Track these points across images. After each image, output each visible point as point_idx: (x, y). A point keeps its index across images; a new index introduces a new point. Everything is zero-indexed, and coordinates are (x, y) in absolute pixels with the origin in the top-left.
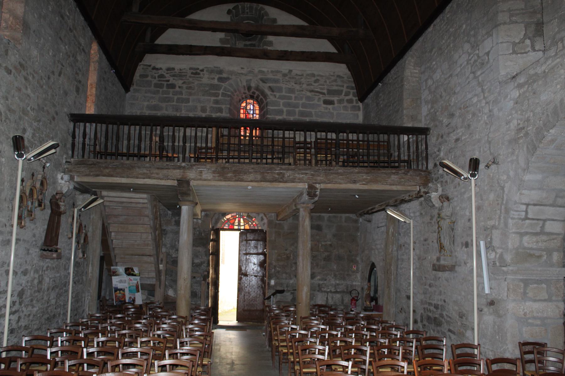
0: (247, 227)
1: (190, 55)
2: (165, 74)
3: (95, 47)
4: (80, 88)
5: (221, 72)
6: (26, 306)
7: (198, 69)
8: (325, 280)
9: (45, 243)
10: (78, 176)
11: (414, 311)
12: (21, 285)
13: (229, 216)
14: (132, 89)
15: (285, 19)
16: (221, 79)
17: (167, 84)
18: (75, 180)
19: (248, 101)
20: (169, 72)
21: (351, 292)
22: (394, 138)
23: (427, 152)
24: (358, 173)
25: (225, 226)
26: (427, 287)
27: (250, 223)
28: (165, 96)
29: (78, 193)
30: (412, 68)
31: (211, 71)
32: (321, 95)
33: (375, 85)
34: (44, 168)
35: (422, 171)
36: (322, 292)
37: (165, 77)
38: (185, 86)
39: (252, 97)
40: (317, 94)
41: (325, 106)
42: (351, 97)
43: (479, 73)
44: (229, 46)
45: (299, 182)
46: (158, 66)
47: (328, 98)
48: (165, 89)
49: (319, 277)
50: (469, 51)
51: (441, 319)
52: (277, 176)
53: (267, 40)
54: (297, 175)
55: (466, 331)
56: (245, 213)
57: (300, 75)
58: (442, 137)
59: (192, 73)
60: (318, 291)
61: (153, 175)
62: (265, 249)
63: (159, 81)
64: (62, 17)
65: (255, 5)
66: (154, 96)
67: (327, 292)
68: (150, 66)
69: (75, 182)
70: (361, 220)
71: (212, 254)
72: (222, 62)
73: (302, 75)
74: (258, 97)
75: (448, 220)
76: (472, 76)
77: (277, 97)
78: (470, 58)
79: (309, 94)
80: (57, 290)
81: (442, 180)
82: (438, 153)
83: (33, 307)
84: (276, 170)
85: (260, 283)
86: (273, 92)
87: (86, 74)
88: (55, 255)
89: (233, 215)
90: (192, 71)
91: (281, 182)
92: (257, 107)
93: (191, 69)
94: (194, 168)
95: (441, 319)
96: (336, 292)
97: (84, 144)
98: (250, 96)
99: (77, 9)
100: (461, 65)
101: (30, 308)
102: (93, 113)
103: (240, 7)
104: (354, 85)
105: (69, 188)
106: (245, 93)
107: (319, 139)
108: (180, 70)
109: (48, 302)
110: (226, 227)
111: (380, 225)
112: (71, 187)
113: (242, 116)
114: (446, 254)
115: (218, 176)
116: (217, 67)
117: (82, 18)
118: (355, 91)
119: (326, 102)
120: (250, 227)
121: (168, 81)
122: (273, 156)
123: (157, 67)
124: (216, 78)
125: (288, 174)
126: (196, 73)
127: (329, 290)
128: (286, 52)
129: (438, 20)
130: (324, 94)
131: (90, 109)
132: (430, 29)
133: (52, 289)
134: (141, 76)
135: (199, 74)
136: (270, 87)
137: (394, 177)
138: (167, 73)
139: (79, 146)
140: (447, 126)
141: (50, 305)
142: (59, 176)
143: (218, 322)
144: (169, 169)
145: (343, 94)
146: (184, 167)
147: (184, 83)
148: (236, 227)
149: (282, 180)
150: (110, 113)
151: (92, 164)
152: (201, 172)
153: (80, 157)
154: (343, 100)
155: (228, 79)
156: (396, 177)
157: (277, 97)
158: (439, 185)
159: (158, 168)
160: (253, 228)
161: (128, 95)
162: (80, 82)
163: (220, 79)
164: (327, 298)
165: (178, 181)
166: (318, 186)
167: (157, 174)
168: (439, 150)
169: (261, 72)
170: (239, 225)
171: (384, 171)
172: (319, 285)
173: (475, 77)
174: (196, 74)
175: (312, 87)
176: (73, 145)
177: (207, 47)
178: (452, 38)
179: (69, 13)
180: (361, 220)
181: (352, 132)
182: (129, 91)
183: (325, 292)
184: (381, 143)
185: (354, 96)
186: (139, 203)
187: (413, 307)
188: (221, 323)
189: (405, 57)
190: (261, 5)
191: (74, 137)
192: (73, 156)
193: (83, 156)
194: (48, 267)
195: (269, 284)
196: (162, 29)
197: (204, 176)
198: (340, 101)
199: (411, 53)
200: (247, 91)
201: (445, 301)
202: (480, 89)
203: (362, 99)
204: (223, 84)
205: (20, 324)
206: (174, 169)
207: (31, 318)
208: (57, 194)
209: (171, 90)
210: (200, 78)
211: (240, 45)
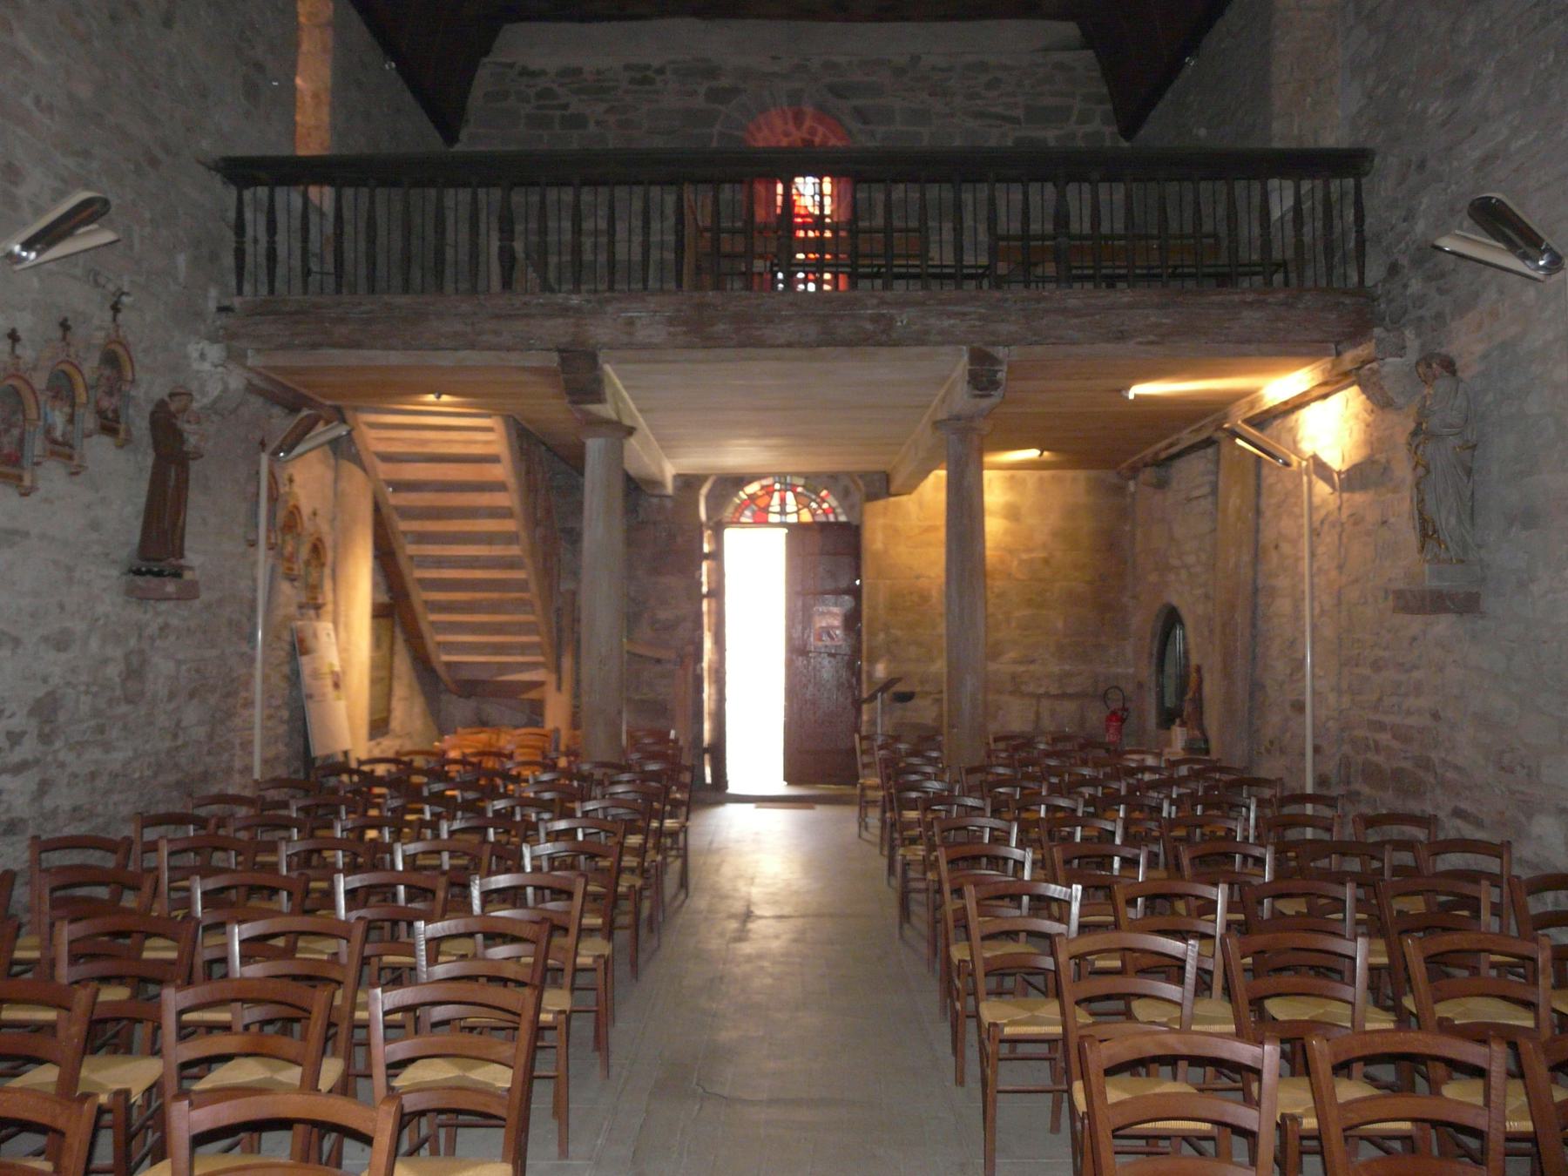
0: (806, 517)
2: (555, 86)
5: (712, 72)
6: (79, 747)
7: (648, 67)
8: (1033, 662)
9: (144, 550)
10: (258, 351)
11: (1317, 750)
12: (45, 680)
13: (753, 488)
16: (715, 95)
17: (563, 116)
18: (250, 362)
21: (1106, 694)
24: (1130, 306)
25: (741, 514)
26: (1367, 671)
27: (814, 505)
29: (277, 411)
33: (1175, 68)
34: (116, 308)
35: (1345, 293)
36: (1023, 695)
45: (942, 344)
46: (535, 64)
49: (1012, 655)
51: (1421, 773)
52: (869, 326)
54: (932, 321)
55: (1530, 817)
56: (798, 474)
57: (942, 70)
60: (1012, 693)
61: (485, 338)
62: (859, 577)
63: (539, 107)
67: (1039, 697)
68: (511, 66)
69: (250, 369)
70: (1132, 486)
71: (709, 595)
75: (1453, 441)
80: (213, 700)
81: (1421, 312)
83: (107, 747)
85: (844, 674)
86: (866, 122)
87: (287, 52)
88: (171, 587)
89: (765, 482)
91: (881, 345)
93: (627, 67)
94: (609, 309)
95: (1421, 773)
96: (1063, 696)
101: (95, 753)
104: (1105, 90)
105: (226, 385)
107: (1003, 238)
109: (175, 736)
110: (747, 517)
111: (1196, 493)
112: (236, 382)
114: (1443, 555)
115: (685, 333)
118: (1109, 107)
120: (814, 514)
121: (565, 107)
124: (702, 90)
125: (903, 319)
126: (643, 77)
127: (1042, 691)
130: (1015, 121)
133: (192, 695)
135: (651, 82)
136: (855, 108)
137: (1250, 317)
138: (561, 85)
139: (256, 254)
140: (1443, 124)
141: (185, 745)
142: (193, 350)
143: (726, 787)
145: (1074, 118)
146: (578, 309)
148: (774, 518)
149: (884, 338)
150: (345, 152)
152: (631, 322)
155: (734, 91)
156: (1257, 315)
158: (1409, 333)
159: (498, 317)
160: (822, 519)
163: (715, 95)
164: (1038, 714)
165: (560, 351)
166: (1000, 352)
167: (497, 333)
168: (1409, 217)
170: (783, 512)
171: (1218, 298)
172: (1014, 677)
174: (645, 81)
176: (240, 254)
180: (1132, 486)
183: (1031, 695)
186: (475, 442)
187: (1315, 736)
188: (732, 789)
191: (240, 228)
192: (240, 291)
194: (164, 628)
195: (870, 675)
197: (641, 335)
200: (791, 127)
201: (1436, 716)
205: (48, 803)
207: (101, 783)
208: (172, 395)
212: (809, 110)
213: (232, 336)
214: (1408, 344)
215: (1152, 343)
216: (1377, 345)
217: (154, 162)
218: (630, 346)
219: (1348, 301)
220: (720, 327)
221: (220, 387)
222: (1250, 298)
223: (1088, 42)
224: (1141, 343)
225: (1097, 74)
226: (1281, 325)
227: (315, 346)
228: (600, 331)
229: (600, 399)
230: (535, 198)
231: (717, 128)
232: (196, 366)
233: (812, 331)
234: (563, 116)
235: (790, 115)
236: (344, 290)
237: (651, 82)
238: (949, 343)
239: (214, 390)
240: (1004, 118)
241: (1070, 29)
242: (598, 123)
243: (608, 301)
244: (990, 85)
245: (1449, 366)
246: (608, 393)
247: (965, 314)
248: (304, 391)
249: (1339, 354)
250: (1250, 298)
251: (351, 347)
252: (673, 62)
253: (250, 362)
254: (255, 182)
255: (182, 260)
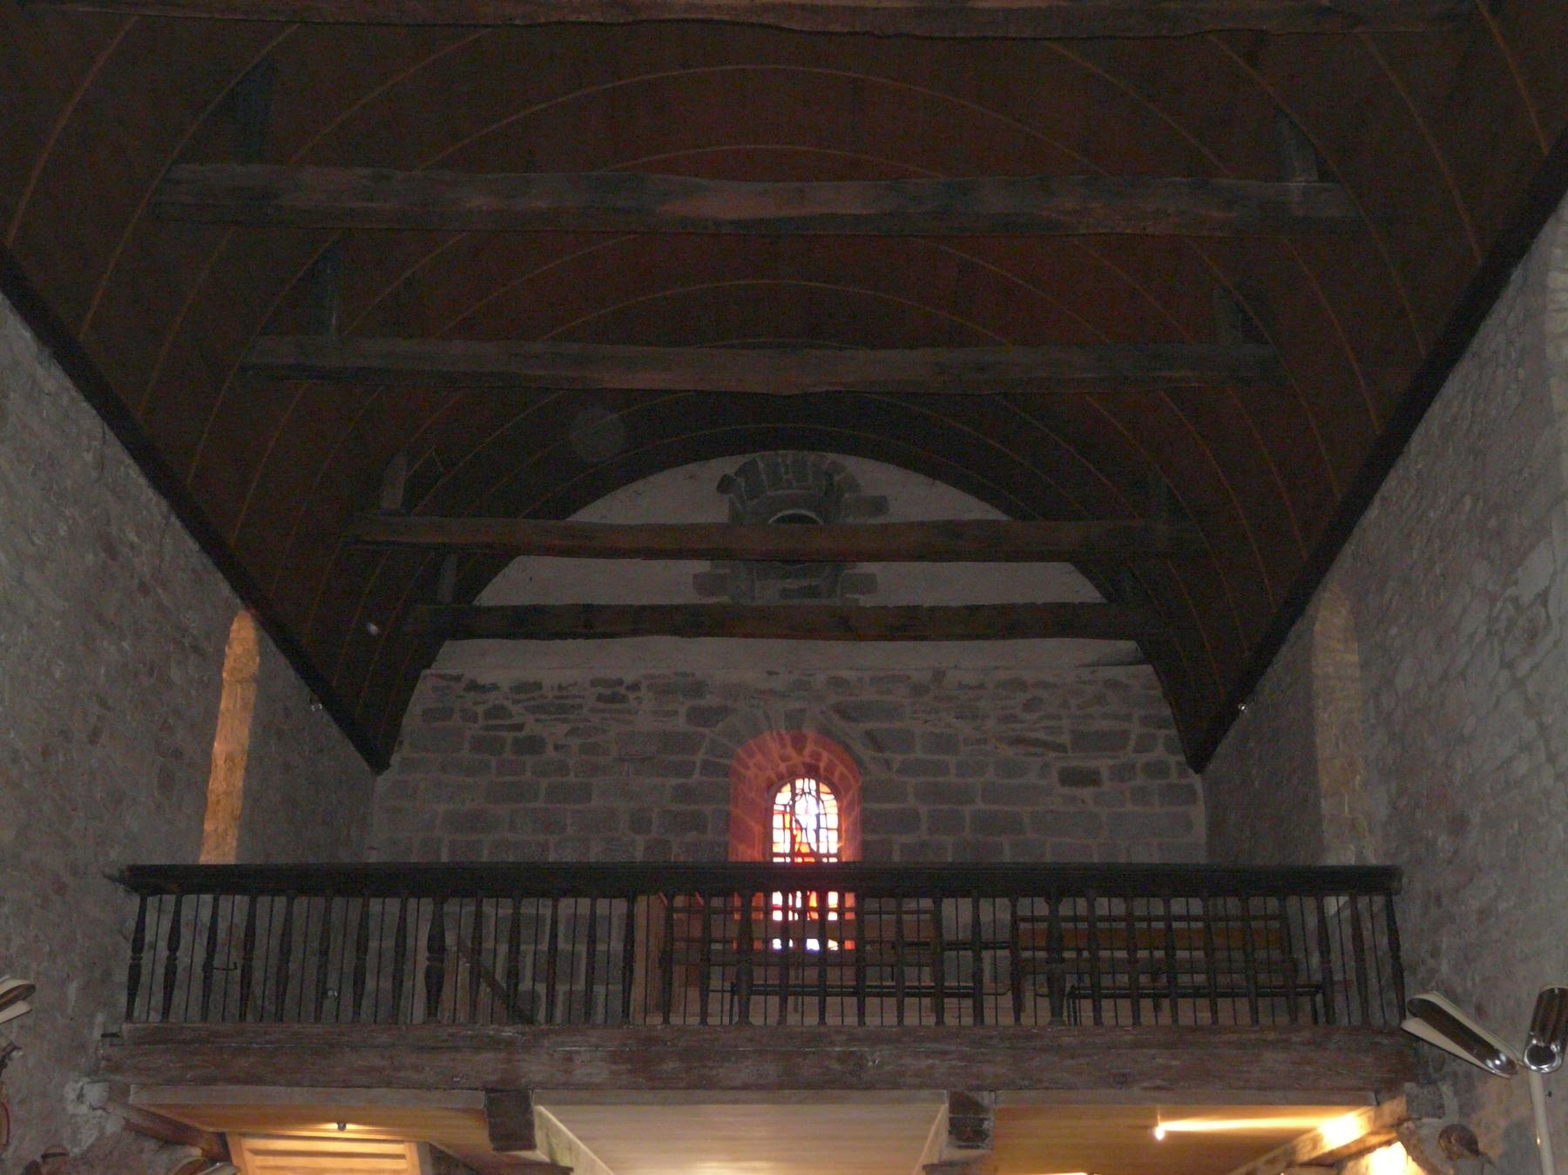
1: (587, 637)
2: (508, 704)
3: (244, 634)
4: (182, 773)
5: (697, 689)
7: (620, 682)
14: (395, 759)
15: (919, 499)
16: (701, 716)
17: (516, 741)
19: (799, 783)
20: (522, 696)
22: (1302, 911)
23: (1396, 957)
28: (509, 779)
29: (150, 1145)
30: (1340, 646)
31: (664, 690)
32: (1052, 754)
37: (511, 716)
38: (575, 742)
39: (811, 772)
40: (1039, 750)
41: (1066, 790)
42: (1158, 752)
43: (1524, 667)
44: (725, 599)
45: (920, 1087)
46: (485, 679)
47: (1076, 762)
48: (508, 755)
50: (1490, 588)
52: (837, 1067)
53: (856, 571)
54: (908, 1061)
58: (1438, 899)
59: (600, 698)
61: (402, 1074)
63: (487, 728)
64: (111, 551)
65: (811, 457)
66: (470, 780)
68: (458, 678)
69: (133, 1108)
72: (704, 657)
73: (981, 686)
74: (830, 768)
76: (1504, 676)
77: (895, 766)
78: (1495, 611)
79: (1010, 752)
82: (1431, 962)
84: (832, 1043)
86: (880, 749)
90: (601, 690)
92: (830, 803)
93: (595, 683)
97: (208, 966)
98: (805, 764)
99: (173, 519)
100: (1471, 637)
102: (231, 860)
103: (761, 466)
105: (102, 1130)
106: (784, 759)
108: (560, 687)
112: (113, 1126)
113: (781, 843)
115: (630, 1072)
116: (685, 675)
117: (192, 545)
118: (1173, 732)
119: (1072, 778)
121: (520, 727)
122: (939, 977)
123: (481, 681)
124: (683, 710)
126: (614, 695)
128: (913, 610)
129: (1391, 483)
131: (219, 847)
132: (1373, 512)
134: (428, 715)
135: (623, 699)
136: (868, 733)
137: (1274, 1059)
138: (515, 702)
139: (154, 962)
142: (70, 1093)
144: (456, 1049)
145: (1130, 748)
146: (510, 1043)
147: (572, 732)
151: (192, 1041)
152: (569, 1058)
153: (155, 1017)
154: (1133, 766)
155: (724, 711)
156: (1281, 1056)
157: (895, 766)
158: (1446, 1089)
161: (383, 782)
162: (178, 754)
163: (701, 716)
165: (489, 1090)
166: (986, 1098)
167: (418, 1069)
169: (837, 683)
173: (1517, 683)
174: (614, 699)
175: (1018, 726)
177: (643, 608)
178: (1437, 544)
179: (138, 534)
181: (1110, 893)
182: (387, 766)
184: (1254, 924)
185: (1170, 749)
189: (1310, 610)
190: (831, 456)
193: (166, 1012)
196: (497, 558)
197: (580, 1074)
198: (1123, 773)
199: (1327, 595)
200: (790, 751)
202: (1532, 725)
203: (1199, 758)
204: (707, 731)
206: (478, 1050)
208: (44, 1157)
209: (529, 760)
210: (629, 712)
211: (769, 592)
212: (809, 731)
213: (116, 1068)
214: (1446, 1102)
215: (1158, 1088)
216: (1409, 1103)
217: (61, 889)
218: (566, 1085)
219: (1386, 1042)
220: (670, 1066)
221: (96, 1133)
222: (1271, 1036)
223: (1150, 654)
224: (1145, 1089)
225: (1157, 693)
226: (1308, 1069)
227: (208, 1081)
228: (534, 1068)
229: (531, 1146)
230: (470, 908)
231: (699, 757)
232: (71, 1109)
233: (771, 1070)
234: (516, 741)
235: (787, 738)
236: (249, 1018)
237: (623, 699)
238: (928, 1086)
239: (88, 1137)
240: (1045, 744)
241: (1127, 646)
242: (557, 748)
243: (545, 1034)
244: (1028, 706)
245: (1471, 1144)
246: (539, 1136)
247: (945, 1053)
248: (187, 1121)
249: (1378, 1104)
250: (1271, 1036)
251: (252, 1083)
252: (652, 677)
253: (131, 1100)
254: (158, 891)
255: (73, 989)
